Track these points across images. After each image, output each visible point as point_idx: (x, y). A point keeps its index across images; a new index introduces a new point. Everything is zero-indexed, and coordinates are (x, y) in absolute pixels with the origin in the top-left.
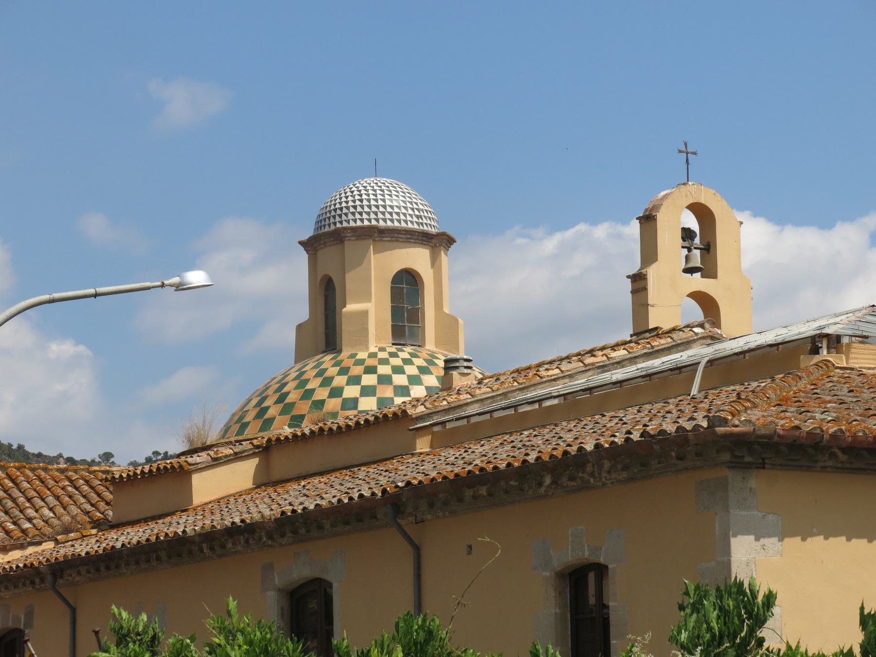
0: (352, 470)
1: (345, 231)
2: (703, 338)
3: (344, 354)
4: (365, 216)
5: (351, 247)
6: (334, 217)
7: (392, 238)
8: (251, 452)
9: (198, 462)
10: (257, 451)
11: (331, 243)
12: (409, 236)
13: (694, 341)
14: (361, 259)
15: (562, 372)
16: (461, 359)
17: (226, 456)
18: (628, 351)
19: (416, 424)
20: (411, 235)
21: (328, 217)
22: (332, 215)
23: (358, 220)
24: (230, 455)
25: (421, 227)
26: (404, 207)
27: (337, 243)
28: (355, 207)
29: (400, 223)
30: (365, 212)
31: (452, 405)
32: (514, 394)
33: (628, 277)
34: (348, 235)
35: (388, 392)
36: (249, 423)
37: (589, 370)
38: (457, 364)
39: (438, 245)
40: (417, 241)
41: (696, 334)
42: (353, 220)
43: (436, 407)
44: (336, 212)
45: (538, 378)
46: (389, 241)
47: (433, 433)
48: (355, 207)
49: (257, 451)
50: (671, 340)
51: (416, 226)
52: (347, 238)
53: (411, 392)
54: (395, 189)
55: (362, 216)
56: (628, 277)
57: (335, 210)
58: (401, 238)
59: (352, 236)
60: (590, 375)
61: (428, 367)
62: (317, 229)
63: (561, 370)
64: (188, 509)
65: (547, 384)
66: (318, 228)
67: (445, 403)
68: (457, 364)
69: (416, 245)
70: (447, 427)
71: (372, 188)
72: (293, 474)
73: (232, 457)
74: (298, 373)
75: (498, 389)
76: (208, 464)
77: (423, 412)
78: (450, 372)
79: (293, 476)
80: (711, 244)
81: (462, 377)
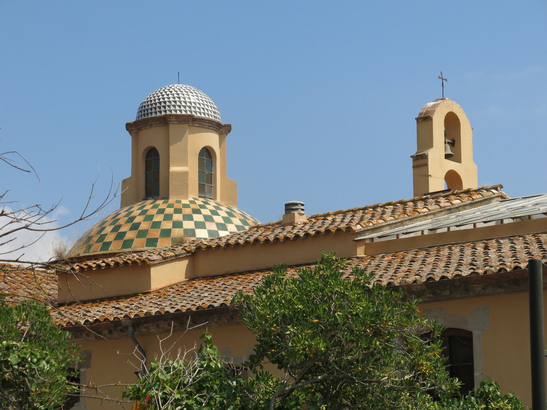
0: (309, 266)
1: (171, 117)
2: (497, 197)
3: (171, 200)
4: (182, 108)
5: (173, 128)
6: (151, 109)
7: (200, 124)
8: (185, 255)
9: (155, 259)
10: (188, 255)
11: (157, 125)
12: (210, 125)
13: (493, 198)
14: (180, 138)
15: (429, 210)
16: (300, 204)
17: (171, 257)
18: (461, 201)
19: (357, 237)
20: (212, 124)
21: (150, 108)
22: (153, 107)
23: (178, 110)
24: (173, 256)
25: (216, 119)
26: (202, 104)
27: (161, 125)
28: (165, 102)
29: (201, 114)
30: (182, 106)
31: (376, 226)
32: (407, 222)
33: (411, 157)
34: (172, 120)
35: (213, 227)
36: (111, 242)
37: (443, 211)
38: (297, 207)
39: (224, 133)
40: (214, 128)
41: (494, 194)
42: (174, 110)
43: (367, 226)
44: (161, 104)
45: (417, 213)
46: (198, 126)
47: (366, 244)
48: (175, 102)
49: (188, 255)
50: (481, 196)
51: (213, 118)
52: (172, 122)
53: (227, 227)
54: (192, 94)
55: (180, 108)
56: (411, 157)
57: (152, 105)
58: (206, 125)
59: (175, 121)
60: (443, 214)
61: (133, 224)
62: (138, 117)
63: (428, 209)
64: (150, 292)
65: (423, 218)
66: (139, 116)
67: (371, 224)
68: (297, 207)
69: (213, 131)
70: (374, 242)
71: (176, 93)
72: (221, 272)
73: (173, 258)
74: (127, 212)
75: (398, 218)
76: (161, 262)
77: (360, 229)
78: (292, 212)
79: (220, 274)
80: (455, 140)
81: (300, 216)
